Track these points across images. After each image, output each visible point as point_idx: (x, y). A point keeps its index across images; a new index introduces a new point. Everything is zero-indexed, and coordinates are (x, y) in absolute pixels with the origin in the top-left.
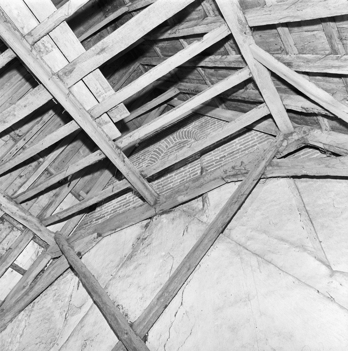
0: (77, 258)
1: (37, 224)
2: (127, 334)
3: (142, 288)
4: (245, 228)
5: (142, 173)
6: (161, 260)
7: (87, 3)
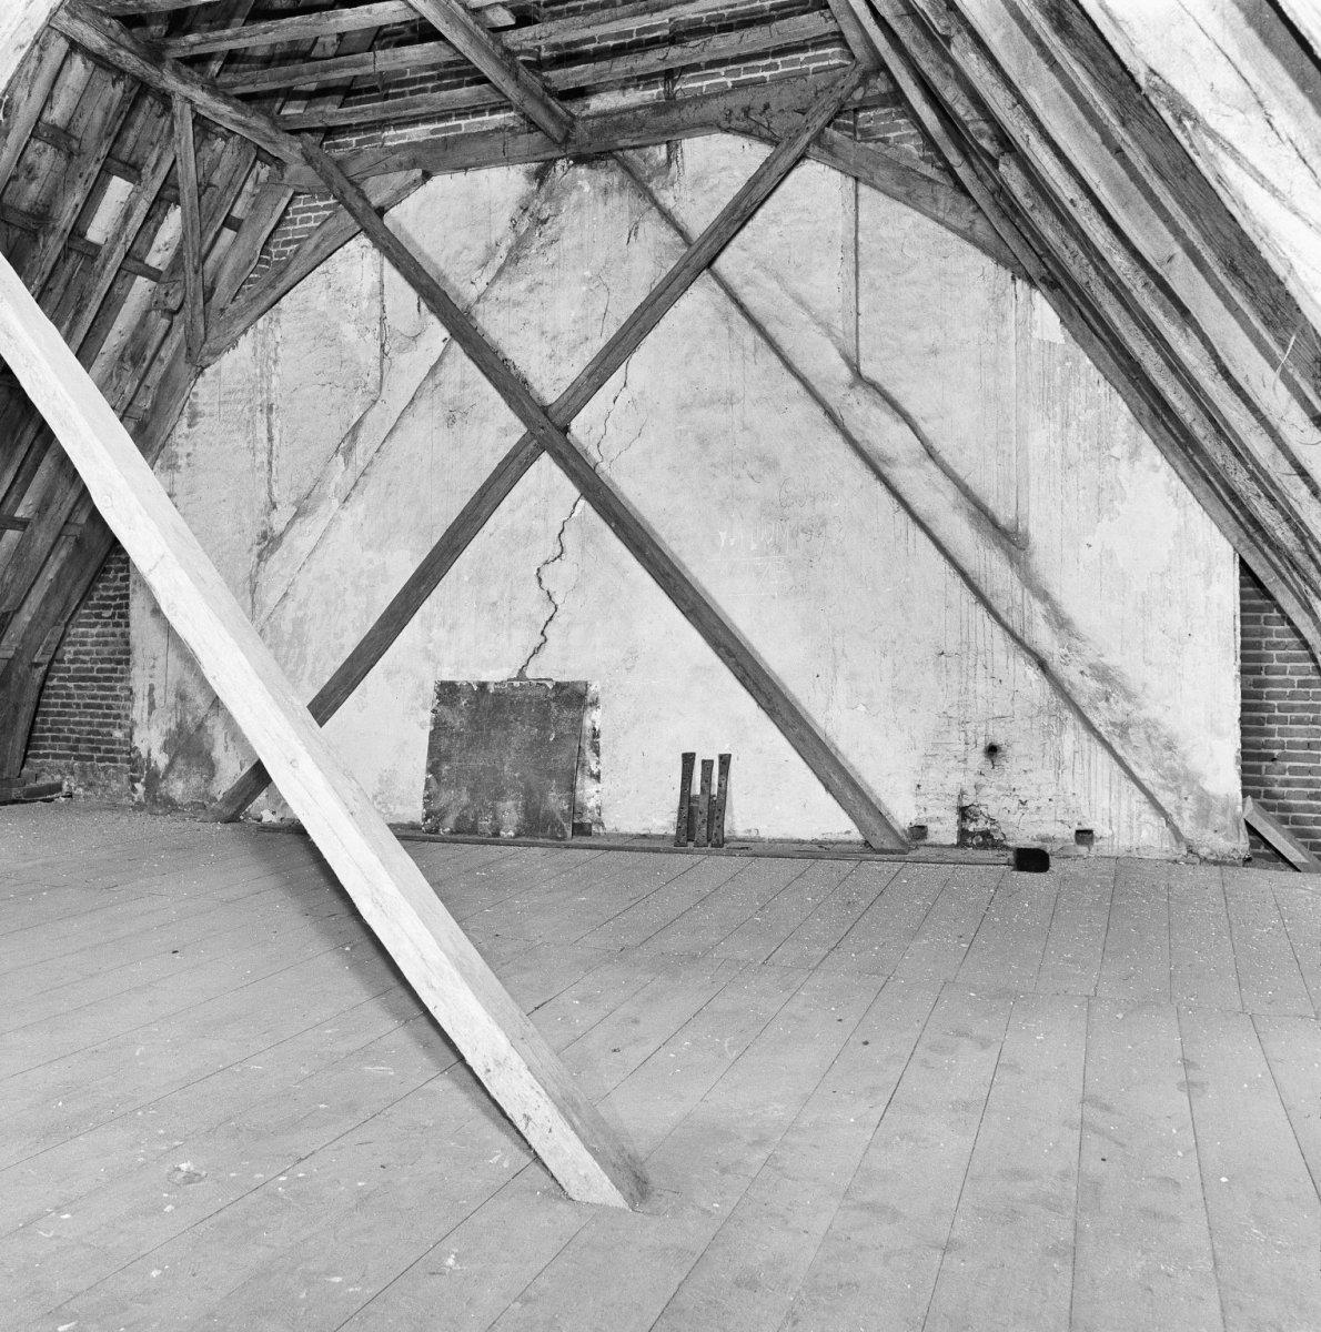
0: (375, 218)
1: (267, 131)
2: (543, 428)
3: (550, 335)
4: (745, 255)
5: (548, 85)
6: (584, 288)
7: (800, 754)
